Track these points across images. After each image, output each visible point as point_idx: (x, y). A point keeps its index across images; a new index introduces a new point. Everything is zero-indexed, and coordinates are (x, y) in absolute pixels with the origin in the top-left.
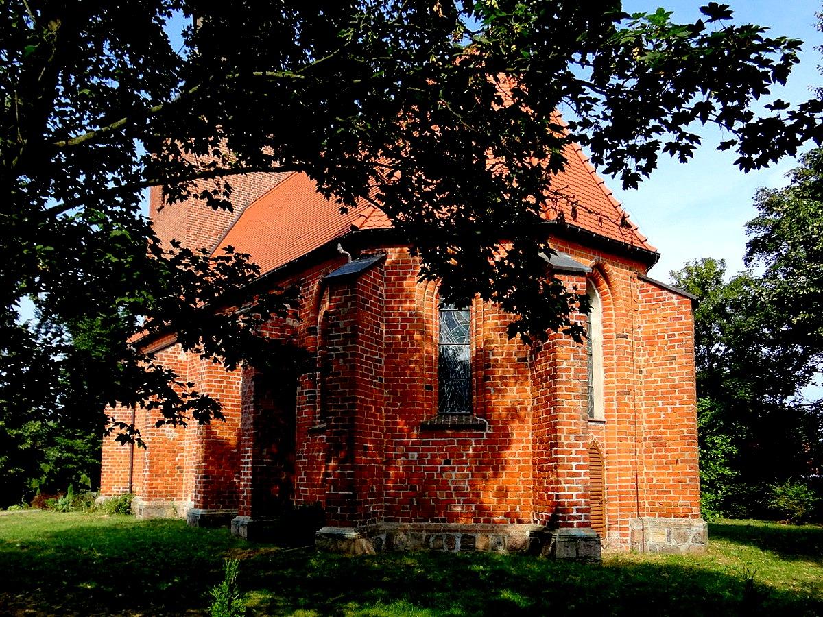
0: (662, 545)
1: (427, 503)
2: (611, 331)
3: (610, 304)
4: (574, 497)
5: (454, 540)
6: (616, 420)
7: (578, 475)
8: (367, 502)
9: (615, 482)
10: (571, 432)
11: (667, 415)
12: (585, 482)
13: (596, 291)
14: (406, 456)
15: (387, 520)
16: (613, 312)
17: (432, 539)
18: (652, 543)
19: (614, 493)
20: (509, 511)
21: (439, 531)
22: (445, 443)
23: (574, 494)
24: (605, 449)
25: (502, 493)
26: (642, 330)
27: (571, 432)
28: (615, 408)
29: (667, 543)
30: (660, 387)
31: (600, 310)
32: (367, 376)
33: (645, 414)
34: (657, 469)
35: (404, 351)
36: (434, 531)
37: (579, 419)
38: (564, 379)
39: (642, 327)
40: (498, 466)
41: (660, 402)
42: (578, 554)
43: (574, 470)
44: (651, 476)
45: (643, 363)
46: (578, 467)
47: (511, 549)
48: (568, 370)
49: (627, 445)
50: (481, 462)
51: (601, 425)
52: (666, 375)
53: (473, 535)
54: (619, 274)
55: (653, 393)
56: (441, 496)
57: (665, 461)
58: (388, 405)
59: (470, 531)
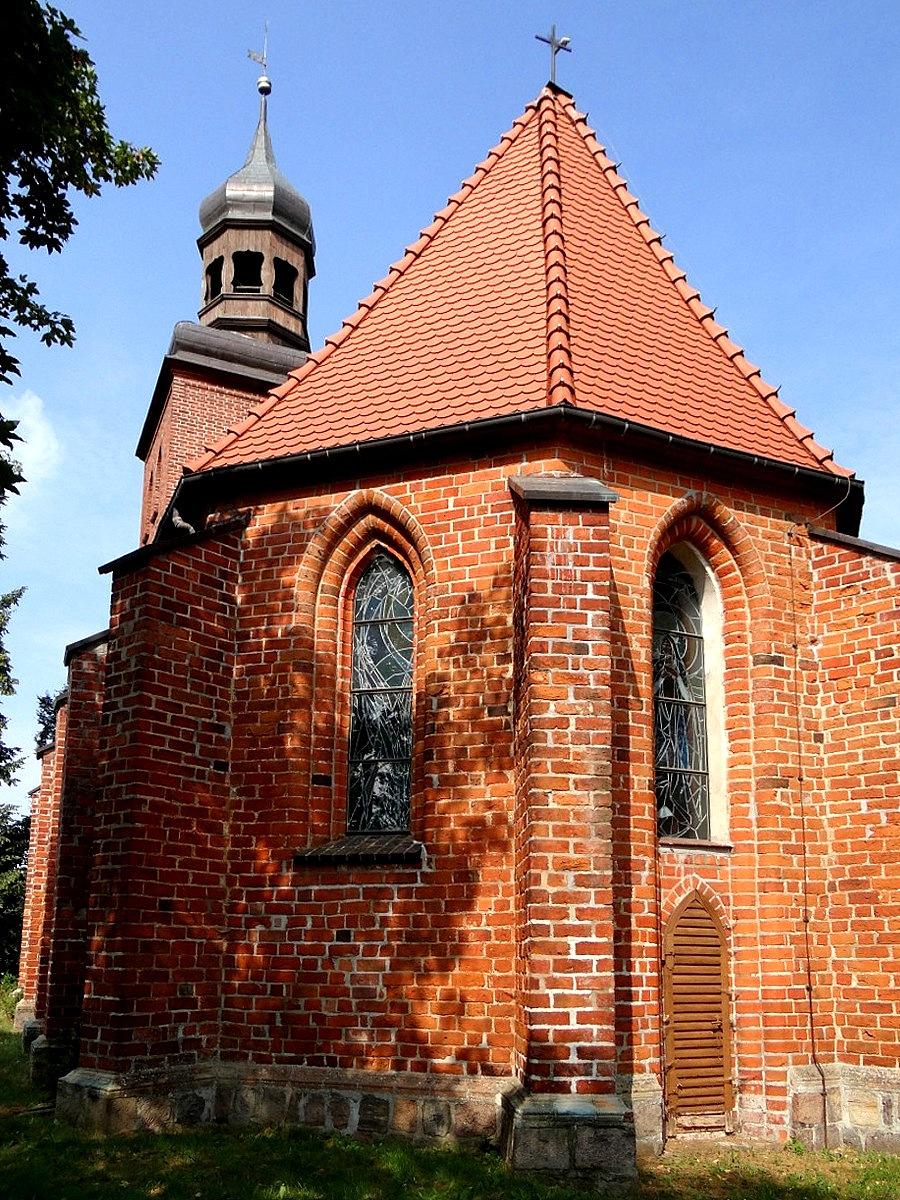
0: (872, 1131)
1: (302, 1025)
2: (741, 651)
3: (739, 592)
4: (573, 1019)
5: (348, 1107)
6: (756, 843)
7: (583, 966)
8: (166, 1018)
9: (756, 982)
10: (565, 865)
11: (877, 830)
12: (600, 983)
13: (708, 569)
14: (266, 922)
15: (226, 1057)
16: (747, 609)
17: (302, 1102)
18: (849, 1126)
19: (754, 1008)
20: (466, 1045)
21: (317, 1086)
22: (339, 894)
24: (732, 908)
25: (454, 1008)
26: (820, 646)
27: (565, 865)
28: (753, 815)
29: (883, 1128)
30: (863, 769)
31: (719, 607)
32: (176, 757)
33: (830, 831)
34: (859, 953)
35: (270, 706)
36: (308, 1084)
37: (585, 834)
38: (551, 744)
39: (821, 639)
40: (447, 950)
41: (864, 803)
42: (573, 1160)
43: (573, 955)
44: (846, 970)
45: (824, 718)
46: (582, 948)
47: (464, 1135)
48: (562, 723)
49: (782, 900)
50: (410, 937)
51: (719, 855)
52: (875, 741)
53: (385, 1097)
54: (757, 530)
55: (845, 784)
56: (329, 1009)
57: (876, 935)
58: (237, 817)
59: (378, 1088)
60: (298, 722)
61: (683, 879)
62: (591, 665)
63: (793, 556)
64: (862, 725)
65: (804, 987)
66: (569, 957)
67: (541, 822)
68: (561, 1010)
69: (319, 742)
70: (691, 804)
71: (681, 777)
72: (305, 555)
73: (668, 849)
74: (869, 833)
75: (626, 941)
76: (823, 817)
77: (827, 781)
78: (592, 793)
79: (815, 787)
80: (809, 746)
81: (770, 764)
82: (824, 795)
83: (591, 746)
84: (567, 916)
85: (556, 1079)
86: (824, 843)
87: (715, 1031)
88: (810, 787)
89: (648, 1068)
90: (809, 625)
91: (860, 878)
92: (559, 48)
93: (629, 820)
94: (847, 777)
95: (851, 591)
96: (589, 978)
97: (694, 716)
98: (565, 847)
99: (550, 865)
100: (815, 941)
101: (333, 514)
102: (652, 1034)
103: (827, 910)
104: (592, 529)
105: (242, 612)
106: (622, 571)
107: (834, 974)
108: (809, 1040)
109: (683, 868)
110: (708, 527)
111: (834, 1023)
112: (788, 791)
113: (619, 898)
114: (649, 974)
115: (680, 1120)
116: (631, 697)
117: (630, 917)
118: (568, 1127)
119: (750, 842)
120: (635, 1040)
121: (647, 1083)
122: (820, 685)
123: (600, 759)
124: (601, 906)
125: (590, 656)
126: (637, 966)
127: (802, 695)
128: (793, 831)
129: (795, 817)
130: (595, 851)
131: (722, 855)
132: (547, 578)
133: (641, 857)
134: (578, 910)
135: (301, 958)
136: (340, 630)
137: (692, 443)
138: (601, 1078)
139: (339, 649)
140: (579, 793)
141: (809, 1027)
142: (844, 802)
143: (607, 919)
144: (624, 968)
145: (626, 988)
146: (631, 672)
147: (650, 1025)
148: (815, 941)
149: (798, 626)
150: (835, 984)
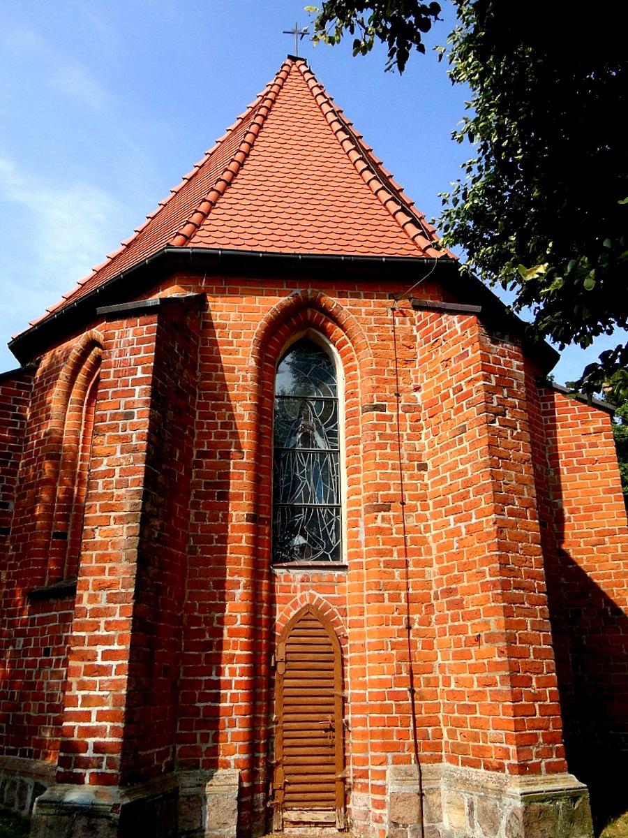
7: (104, 671)
10: (101, 586)
23: (94, 710)
27: (101, 586)
37: (118, 560)
38: (100, 490)
43: (99, 662)
46: (107, 655)
51: (337, 573)
60: (44, 496)
61: (299, 595)
62: (135, 427)
63: (397, 325)
64: (448, 452)
65: (406, 689)
66: (96, 663)
67: (87, 552)
68: (86, 709)
69: (60, 508)
70: (325, 533)
71: (315, 511)
72: (58, 381)
73: (284, 571)
74: (456, 545)
75: (217, 649)
76: (428, 535)
77: (430, 502)
78: (126, 526)
79: (419, 509)
80: (411, 474)
81: (371, 492)
82: (428, 515)
83: (129, 489)
84: (98, 628)
85: (75, 771)
86: (429, 557)
87: (326, 730)
88: (414, 509)
89: (233, 764)
90: (412, 376)
91: (452, 587)
92: (303, 34)
93: (226, 547)
94: (442, 497)
95: (437, 344)
96: (109, 680)
97: (329, 460)
98: (102, 571)
99: (90, 587)
100: (419, 646)
101: (74, 351)
102: (239, 732)
103: (433, 617)
104: (145, 327)
105: (29, 424)
106: (230, 357)
107: (440, 677)
108: (411, 740)
109: (299, 586)
110: (322, 315)
111: (442, 724)
112: (391, 514)
113: (212, 613)
114: (238, 678)
115: (286, 814)
116: (233, 450)
117: (222, 629)
118: (70, 815)
119: (359, 560)
120: (221, 737)
121: (227, 778)
122: (423, 423)
123: (134, 499)
124: (124, 618)
125: (135, 420)
126: (227, 671)
127: (405, 433)
128: (394, 548)
129: (397, 536)
130: (124, 573)
131: (340, 573)
132: (110, 368)
133: (236, 578)
134: (107, 623)
135: (26, 670)
136: (83, 428)
137: (293, 256)
138: (109, 771)
139: (81, 441)
140: (116, 527)
141: (411, 728)
142: (440, 519)
143: (125, 630)
144: (214, 673)
145: (214, 691)
146: (234, 430)
147: (237, 724)
148: (419, 646)
149: (400, 378)
150: (441, 687)
